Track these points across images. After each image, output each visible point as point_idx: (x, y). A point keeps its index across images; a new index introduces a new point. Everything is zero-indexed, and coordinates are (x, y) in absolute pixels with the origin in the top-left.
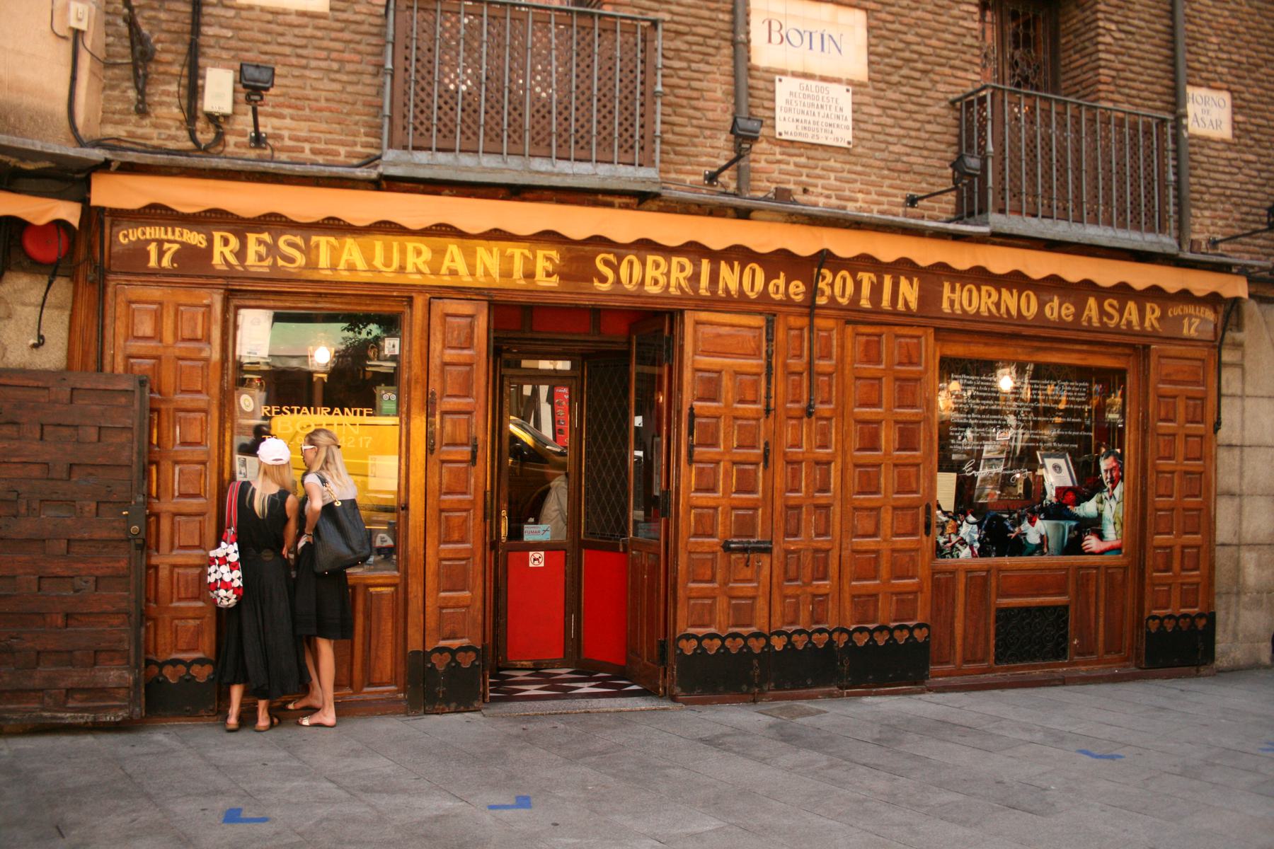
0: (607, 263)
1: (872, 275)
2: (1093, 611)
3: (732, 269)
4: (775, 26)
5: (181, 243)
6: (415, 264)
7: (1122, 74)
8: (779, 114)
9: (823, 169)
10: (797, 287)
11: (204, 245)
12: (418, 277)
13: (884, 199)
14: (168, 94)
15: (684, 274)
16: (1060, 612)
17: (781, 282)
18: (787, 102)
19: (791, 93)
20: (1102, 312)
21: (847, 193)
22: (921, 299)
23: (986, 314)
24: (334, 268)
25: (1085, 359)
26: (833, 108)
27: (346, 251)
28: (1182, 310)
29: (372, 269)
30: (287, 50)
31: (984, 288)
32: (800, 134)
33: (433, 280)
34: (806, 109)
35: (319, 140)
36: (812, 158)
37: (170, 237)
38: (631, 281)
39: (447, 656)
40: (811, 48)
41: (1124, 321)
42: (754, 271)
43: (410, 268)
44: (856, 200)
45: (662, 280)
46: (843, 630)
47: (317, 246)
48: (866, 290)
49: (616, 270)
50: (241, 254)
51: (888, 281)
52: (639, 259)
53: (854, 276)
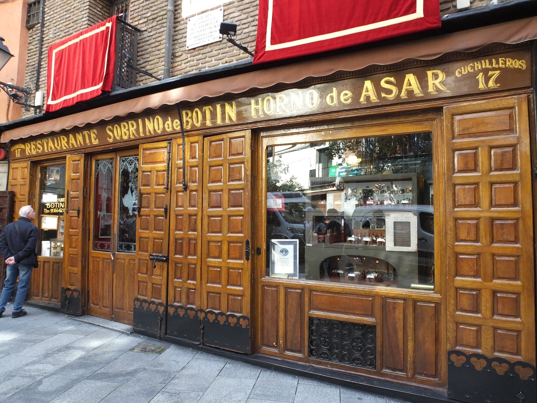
0: (110, 130)
2: (400, 335)
3: (232, 106)
10: (346, 94)
16: (370, 329)
17: (169, 122)
25: (385, 130)
28: (473, 67)
31: (130, 122)
38: (159, 130)
39: (214, 315)
42: (158, 119)
43: (63, 146)
45: (127, 132)
46: (202, 311)
51: (218, 107)
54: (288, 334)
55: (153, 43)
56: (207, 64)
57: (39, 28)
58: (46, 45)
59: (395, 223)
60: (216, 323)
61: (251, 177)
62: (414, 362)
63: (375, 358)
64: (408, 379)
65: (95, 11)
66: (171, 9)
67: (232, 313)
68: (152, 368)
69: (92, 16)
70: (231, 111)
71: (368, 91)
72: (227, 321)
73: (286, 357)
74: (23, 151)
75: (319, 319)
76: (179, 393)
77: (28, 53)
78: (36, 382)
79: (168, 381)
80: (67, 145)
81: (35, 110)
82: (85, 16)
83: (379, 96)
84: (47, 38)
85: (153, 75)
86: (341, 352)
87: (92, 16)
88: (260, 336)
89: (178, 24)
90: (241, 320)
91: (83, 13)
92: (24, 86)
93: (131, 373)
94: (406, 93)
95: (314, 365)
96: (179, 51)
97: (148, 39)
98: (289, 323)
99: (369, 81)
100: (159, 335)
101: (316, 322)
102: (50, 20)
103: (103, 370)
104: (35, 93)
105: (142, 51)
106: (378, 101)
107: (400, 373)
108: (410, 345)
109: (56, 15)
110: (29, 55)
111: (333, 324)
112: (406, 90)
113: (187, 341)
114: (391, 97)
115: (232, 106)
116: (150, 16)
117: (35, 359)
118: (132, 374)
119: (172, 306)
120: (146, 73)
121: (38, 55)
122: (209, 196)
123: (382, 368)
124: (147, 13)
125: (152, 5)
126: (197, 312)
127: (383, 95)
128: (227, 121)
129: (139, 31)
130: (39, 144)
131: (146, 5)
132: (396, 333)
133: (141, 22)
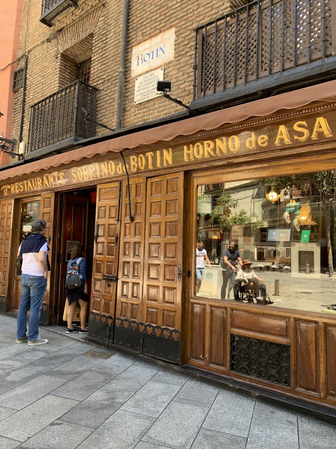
0: (74, 172)
1: (151, 153)
2: (313, 356)
3: (169, 152)
6: (207, 150)
8: (136, 94)
10: (263, 138)
16: (285, 348)
22: (174, 159)
24: (101, 176)
25: (299, 168)
39: (136, 325)
46: (142, 324)
54: (213, 349)
55: (109, 100)
56: (151, 116)
57: (23, 91)
58: (28, 105)
59: (300, 252)
60: (153, 336)
61: (184, 211)
62: (326, 384)
63: (289, 376)
64: (320, 399)
65: (65, 75)
66: (122, 71)
67: (166, 327)
68: (97, 370)
69: (62, 80)
70: (168, 156)
71: (282, 135)
72: (145, 329)
73: (211, 369)
74: (9, 190)
75: (240, 337)
76: (115, 392)
77: (15, 112)
78: (6, 373)
79: (108, 381)
80: (41, 186)
81: (19, 158)
82: (56, 79)
84: (28, 99)
85: (108, 127)
86: (258, 368)
87: (62, 80)
88: (189, 348)
89: (127, 83)
90: (156, 329)
91: (55, 77)
92: (11, 138)
93: (79, 372)
94: (316, 134)
95: (235, 378)
96: (129, 106)
97: (104, 96)
98: (213, 338)
99: (283, 126)
100: (107, 344)
101: (237, 338)
102: (30, 85)
103: (58, 368)
104: (19, 144)
105: (100, 107)
106: (291, 143)
107: (313, 393)
108: (322, 367)
109: (35, 80)
110: (15, 113)
111: (251, 342)
112: (317, 131)
113: (130, 350)
114: (303, 139)
115: (169, 152)
116: (106, 77)
117: (8, 356)
118: (80, 373)
119: (119, 319)
120: (102, 125)
121: (21, 113)
122: (151, 227)
123: (295, 387)
124: (104, 75)
125: (108, 68)
126: (138, 324)
128: (165, 165)
129: (97, 90)
130: (21, 184)
131: (103, 68)
132: (308, 353)
133: (99, 82)
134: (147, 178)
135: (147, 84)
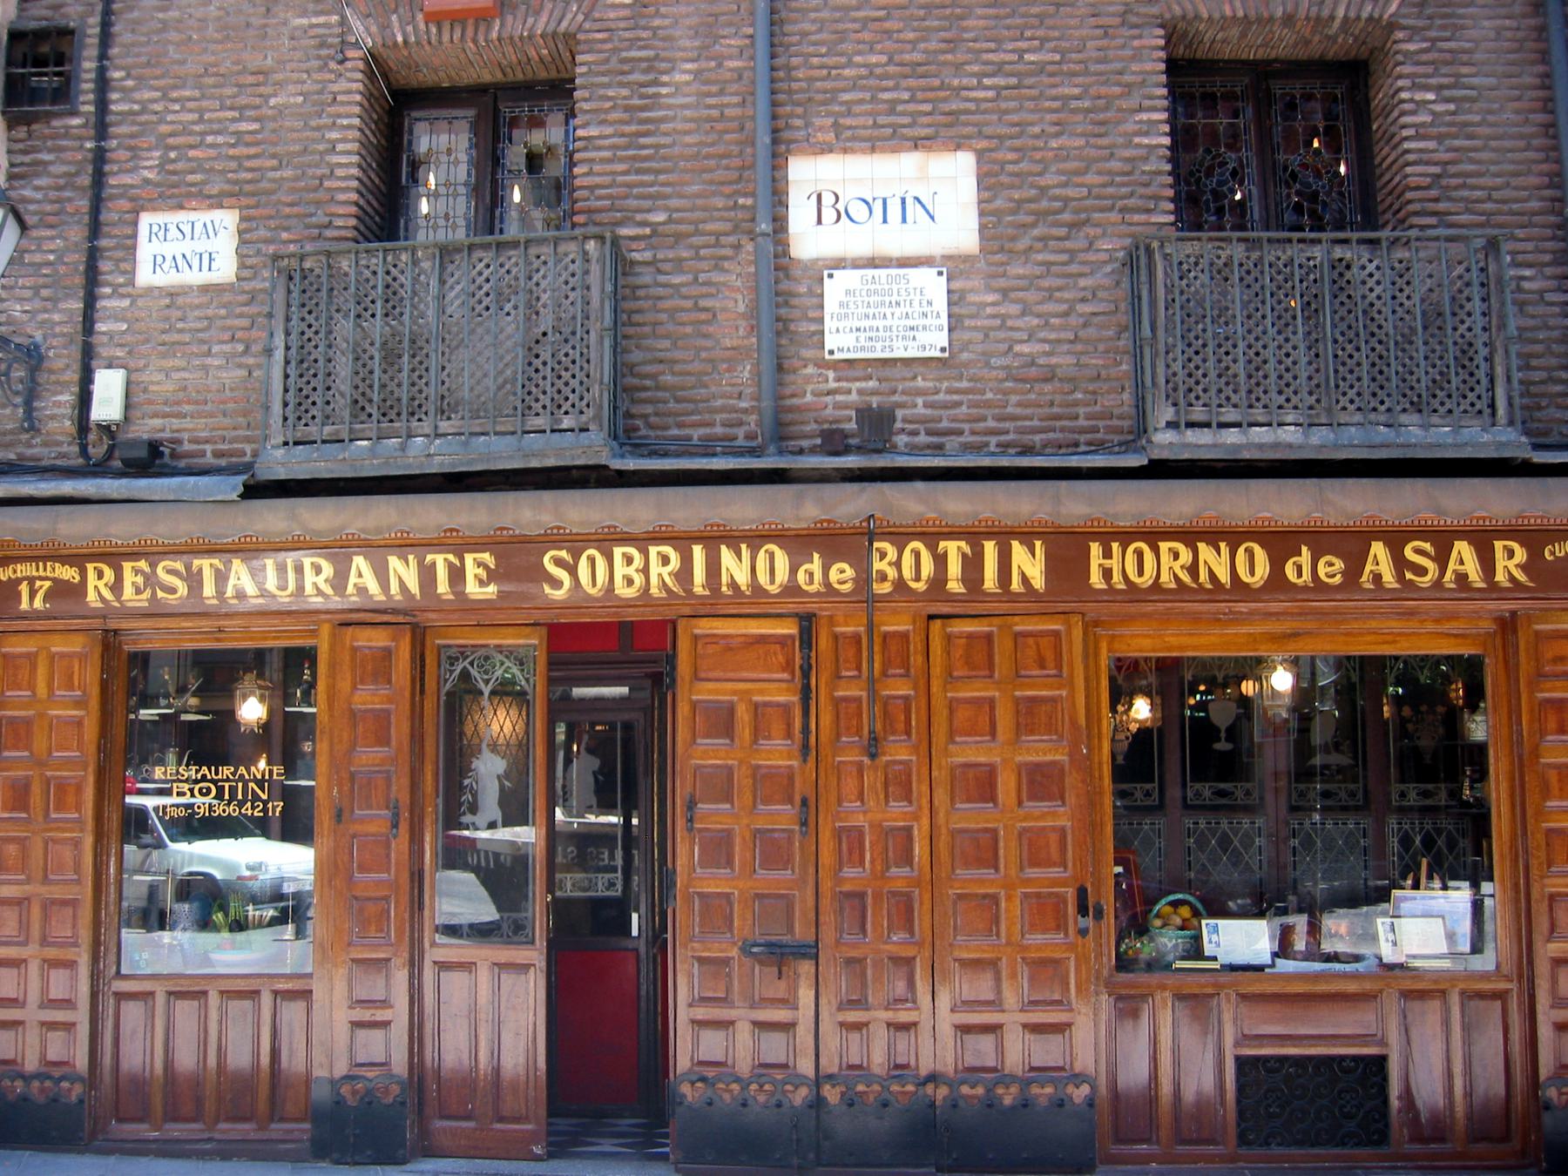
0: (559, 562)
1: (963, 544)
3: (739, 555)
4: (828, 199)
5: (54, 580)
6: (315, 584)
7: (1452, 169)
8: (829, 324)
9: (904, 393)
10: (842, 571)
11: (78, 578)
12: (320, 599)
13: (1007, 425)
14: (58, 404)
15: (669, 568)
17: (816, 565)
18: (841, 305)
19: (848, 292)
20: (1400, 563)
21: (945, 424)
23: (1173, 585)
26: (916, 303)
27: (232, 574)
29: (264, 593)
30: (187, 338)
32: (863, 349)
33: (336, 602)
34: (871, 311)
35: (224, 439)
36: (886, 380)
37: (42, 573)
40: (885, 221)
41: (1449, 575)
42: (772, 555)
43: (309, 589)
44: (960, 433)
47: (200, 570)
48: (954, 568)
49: (573, 570)
50: (117, 587)
52: (602, 553)
53: (932, 548)
83: (1400, 577)
127: (1409, 576)
134: (931, 617)
135: (883, 304)
